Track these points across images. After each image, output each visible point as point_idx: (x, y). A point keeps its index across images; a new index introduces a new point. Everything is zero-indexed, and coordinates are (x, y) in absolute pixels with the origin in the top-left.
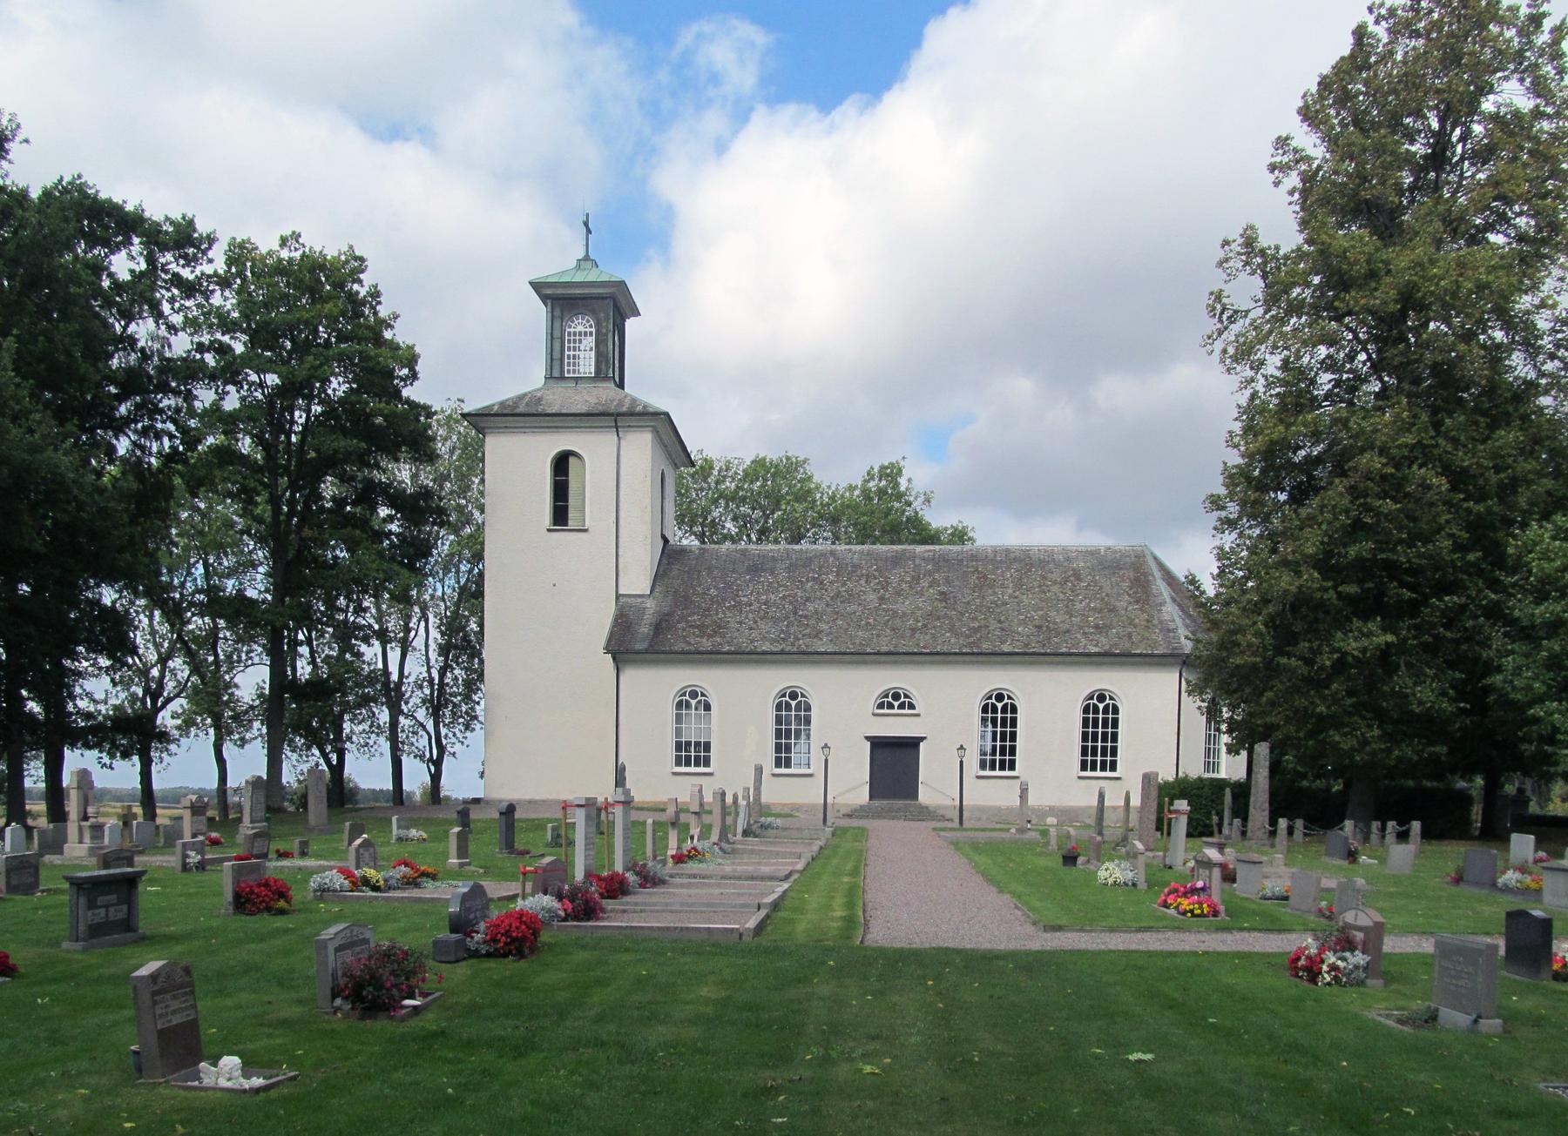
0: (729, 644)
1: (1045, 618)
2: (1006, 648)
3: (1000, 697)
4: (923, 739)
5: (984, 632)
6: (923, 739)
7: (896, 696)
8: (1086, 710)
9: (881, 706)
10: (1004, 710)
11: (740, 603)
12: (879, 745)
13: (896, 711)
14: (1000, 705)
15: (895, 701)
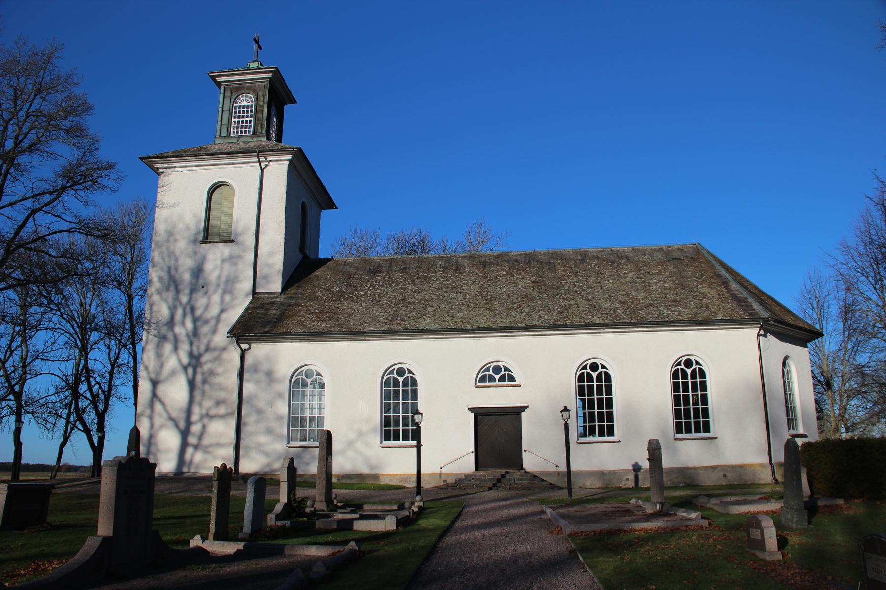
0: (340, 326)
1: (627, 295)
2: (597, 320)
3: (688, 363)
4: (523, 408)
5: (575, 309)
6: (523, 408)
7: (497, 369)
8: (675, 375)
9: (483, 379)
10: (405, 384)
11: (357, 296)
12: (481, 415)
13: (497, 383)
14: (594, 375)
15: (496, 374)
